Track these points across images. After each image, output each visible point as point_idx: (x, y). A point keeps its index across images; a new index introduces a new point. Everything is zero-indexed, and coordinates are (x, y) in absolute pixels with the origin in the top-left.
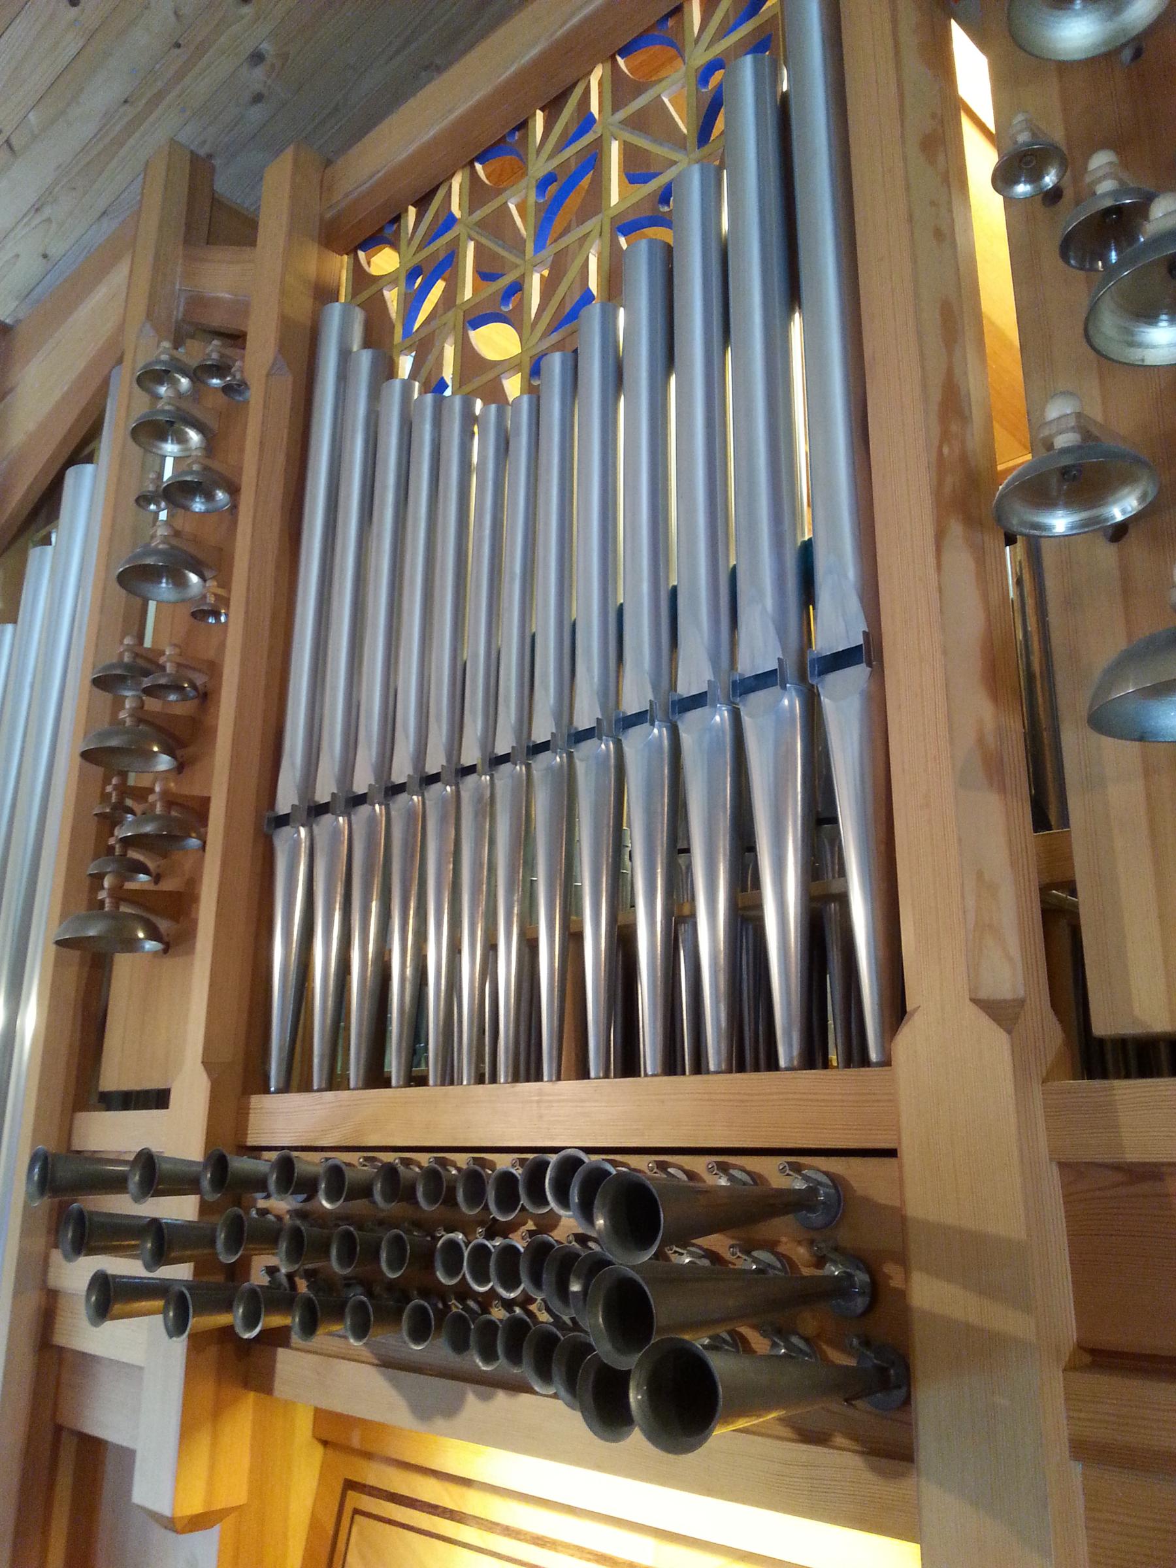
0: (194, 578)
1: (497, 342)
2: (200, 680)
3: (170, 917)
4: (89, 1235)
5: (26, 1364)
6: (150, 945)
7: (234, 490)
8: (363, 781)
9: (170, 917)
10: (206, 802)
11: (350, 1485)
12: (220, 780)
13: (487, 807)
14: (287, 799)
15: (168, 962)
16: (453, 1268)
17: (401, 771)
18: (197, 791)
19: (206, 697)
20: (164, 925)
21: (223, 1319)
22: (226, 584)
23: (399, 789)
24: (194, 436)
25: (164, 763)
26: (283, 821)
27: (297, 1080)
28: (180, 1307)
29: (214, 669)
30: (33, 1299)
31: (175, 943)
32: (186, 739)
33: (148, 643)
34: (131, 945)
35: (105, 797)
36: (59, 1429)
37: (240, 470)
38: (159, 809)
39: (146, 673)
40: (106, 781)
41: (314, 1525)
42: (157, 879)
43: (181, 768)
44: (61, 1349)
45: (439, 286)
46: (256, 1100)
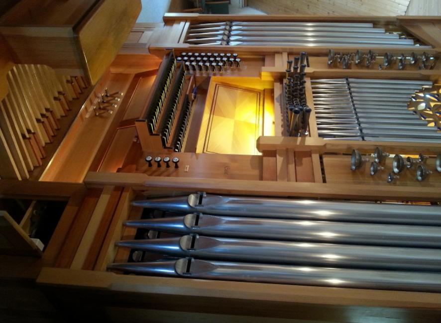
0: (387, 64)
1: (422, 106)
2: (370, 66)
3: (333, 65)
4: (296, 60)
5: (273, 51)
6: (329, 62)
7: (403, 69)
8: (352, 89)
9: (333, 65)
10: (351, 69)
11: (260, 93)
12: (354, 70)
13: (348, 104)
14: (350, 80)
15: (327, 65)
16: (295, 100)
17: (353, 94)
18: (352, 67)
19: (368, 67)
20: (332, 64)
21: (287, 76)
22: (386, 69)
23: (360, 125)
24: (413, 62)
25: (357, 62)
26: (347, 79)
27: (313, 83)
28: (289, 71)
29: (372, 68)
30: (281, 51)
31: (330, 66)
32: (360, 65)
33: (377, 57)
34: (330, 60)
35: (352, 54)
37: (406, 70)
38: (350, 62)
39: (371, 58)
40: (354, 53)
41: (255, 89)
42: (339, 62)
43: (356, 64)
44: (274, 55)
45: (436, 100)
46: (310, 78)
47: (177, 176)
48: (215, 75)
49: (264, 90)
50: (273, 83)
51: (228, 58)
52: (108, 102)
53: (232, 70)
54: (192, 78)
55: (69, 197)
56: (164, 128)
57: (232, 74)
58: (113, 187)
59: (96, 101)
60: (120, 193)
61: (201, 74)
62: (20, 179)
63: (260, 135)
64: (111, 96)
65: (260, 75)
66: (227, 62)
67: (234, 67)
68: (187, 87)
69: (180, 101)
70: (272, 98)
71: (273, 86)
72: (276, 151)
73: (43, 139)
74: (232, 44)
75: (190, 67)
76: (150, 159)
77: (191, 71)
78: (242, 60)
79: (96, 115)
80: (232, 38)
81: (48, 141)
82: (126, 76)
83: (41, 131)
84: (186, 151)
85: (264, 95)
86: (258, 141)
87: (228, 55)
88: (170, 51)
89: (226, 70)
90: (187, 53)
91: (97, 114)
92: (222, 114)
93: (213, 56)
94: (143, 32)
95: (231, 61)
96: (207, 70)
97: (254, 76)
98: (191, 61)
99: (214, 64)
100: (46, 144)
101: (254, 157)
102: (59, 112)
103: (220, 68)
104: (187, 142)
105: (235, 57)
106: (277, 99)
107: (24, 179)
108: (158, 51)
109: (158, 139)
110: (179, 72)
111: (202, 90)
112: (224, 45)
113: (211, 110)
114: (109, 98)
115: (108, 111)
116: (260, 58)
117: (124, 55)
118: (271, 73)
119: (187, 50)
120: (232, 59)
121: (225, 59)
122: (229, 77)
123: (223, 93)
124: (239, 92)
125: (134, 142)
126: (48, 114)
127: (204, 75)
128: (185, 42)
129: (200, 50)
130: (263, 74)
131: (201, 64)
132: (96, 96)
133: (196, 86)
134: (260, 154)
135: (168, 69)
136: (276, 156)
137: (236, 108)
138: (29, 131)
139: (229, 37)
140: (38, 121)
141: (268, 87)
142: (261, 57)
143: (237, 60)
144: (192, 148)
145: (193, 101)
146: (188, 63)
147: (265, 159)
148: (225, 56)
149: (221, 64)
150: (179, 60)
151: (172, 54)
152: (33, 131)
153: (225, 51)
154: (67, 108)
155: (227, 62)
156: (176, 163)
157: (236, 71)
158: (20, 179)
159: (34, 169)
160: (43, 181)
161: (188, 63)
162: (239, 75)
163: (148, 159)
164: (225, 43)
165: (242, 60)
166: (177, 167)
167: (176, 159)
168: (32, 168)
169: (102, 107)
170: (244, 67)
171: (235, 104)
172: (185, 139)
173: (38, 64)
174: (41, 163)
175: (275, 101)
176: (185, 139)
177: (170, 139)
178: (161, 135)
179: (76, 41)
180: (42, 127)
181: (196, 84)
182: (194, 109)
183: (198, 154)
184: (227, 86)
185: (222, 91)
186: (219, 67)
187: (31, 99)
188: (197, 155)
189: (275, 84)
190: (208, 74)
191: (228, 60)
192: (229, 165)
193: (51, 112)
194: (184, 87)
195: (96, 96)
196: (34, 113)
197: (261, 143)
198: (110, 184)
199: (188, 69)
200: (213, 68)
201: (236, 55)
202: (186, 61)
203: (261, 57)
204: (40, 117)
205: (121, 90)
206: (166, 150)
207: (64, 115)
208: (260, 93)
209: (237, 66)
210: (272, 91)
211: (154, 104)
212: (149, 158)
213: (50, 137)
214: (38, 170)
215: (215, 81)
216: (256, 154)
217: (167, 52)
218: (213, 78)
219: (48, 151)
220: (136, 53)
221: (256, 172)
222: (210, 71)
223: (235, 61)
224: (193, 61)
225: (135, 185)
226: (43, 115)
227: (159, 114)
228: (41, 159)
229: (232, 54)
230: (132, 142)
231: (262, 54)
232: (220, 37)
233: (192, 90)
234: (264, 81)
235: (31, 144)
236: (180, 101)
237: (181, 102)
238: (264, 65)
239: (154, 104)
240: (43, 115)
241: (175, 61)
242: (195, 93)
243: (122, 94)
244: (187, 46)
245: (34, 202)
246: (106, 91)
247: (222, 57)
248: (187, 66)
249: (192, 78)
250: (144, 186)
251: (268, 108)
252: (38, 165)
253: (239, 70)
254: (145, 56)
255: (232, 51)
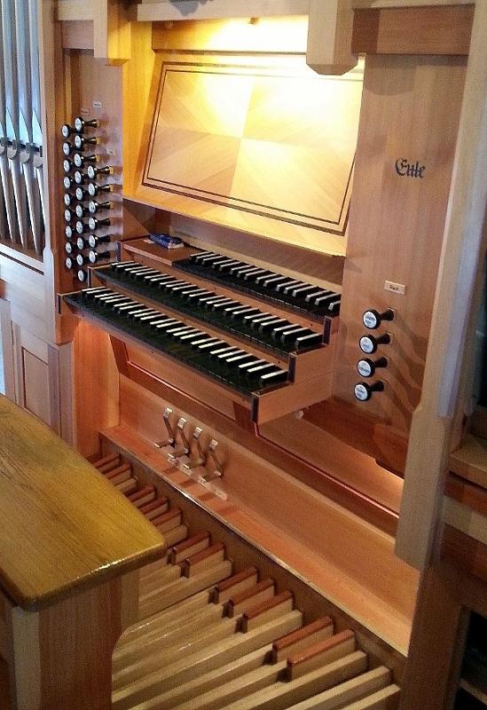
5: (51, 26)
11: (165, 63)
36: (64, 50)
44: (61, 22)
47: (425, 317)
48: (118, 188)
49: (156, 51)
50: (137, 25)
51: (73, 150)
52: (189, 446)
53: (105, 140)
54: (127, 247)
55: (464, 609)
56: (267, 337)
57: (116, 140)
58: (446, 499)
59: (185, 468)
60: (467, 487)
61: (118, 221)
62: (392, 689)
63: (303, 59)
64: (173, 435)
65: (118, 63)
66: (86, 154)
67: (96, 135)
68: (152, 263)
69: (186, 282)
70: (180, 26)
71: (145, 23)
72: (356, 10)
73: (284, 617)
74: (39, 139)
75: (101, 249)
76: (364, 389)
77: (112, 247)
78: (77, 113)
79: (220, 477)
80: (25, 139)
81: (289, 603)
82: (123, 390)
83: (266, 621)
84: (338, 280)
85: (170, 51)
86: (320, 69)
87: (66, 151)
88: (63, 303)
89: (105, 158)
90: (68, 255)
91: (220, 474)
92: (228, 174)
93: (71, 174)
94: (23, 348)
95: (81, 141)
96: (108, 207)
97: (120, 79)
98: (86, 212)
99: (91, 189)
100: (294, 608)
101: (368, 84)
102: (214, 567)
103: (103, 173)
104: (305, 272)
105: (72, 131)
106: (185, 13)
107: (391, 679)
108: (65, 330)
109: (303, 360)
110: (111, 283)
111: (158, 223)
112: (43, 159)
113: (214, 202)
114: (179, 438)
115: (211, 449)
116: (72, 66)
117: (79, 423)
118: (110, 30)
119: (60, 256)
120: (78, 141)
121: (78, 159)
122: (121, 148)
123: (167, 167)
124: (162, 123)
125: (303, 417)
126: (224, 597)
127: (121, 214)
128: (40, 257)
129: (59, 223)
130: (113, 55)
131: (92, 206)
132: (173, 469)
133: (149, 237)
134: (361, 64)
135: (109, 313)
136: (377, 10)
137: (208, 134)
138: (270, 659)
139: (23, 147)
140: (241, 627)
141: (147, 40)
142: (68, 58)
143: (78, 128)
144: (333, 266)
145: (187, 245)
146: (92, 256)
147: (383, 46)
148: (70, 158)
149: (91, 172)
150: (85, 274)
151: (73, 296)
152: (269, 648)
153: (58, 157)
154: (205, 543)
155: (86, 154)
156: (379, 318)
157: (108, 130)
158: (392, 689)
159: (363, 651)
160: (407, 647)
161: (92, 256)
162: (118, 121)
163: (364, 396)
164: (36, 157)
165: (77, 113)
166: (389, 316)
167: (370, 320)
168: (359, 655)
169: (200, 461)
170: (96, 107)
171: (196, 136)
172: (296, 275)
173: (109, 656)
174: (348, 633)
175: (190, 17)
176: (296, 275)
177: (297, 322)
178: (292, 354)
179: (43, 604)
180: (256, 619)
181: (145, 237)
182: (209, 248)
183: (348, 249)
184: (145, 156)
185: (157, 171)
186: (98, 176)
187: (190, 642)
188: (351, 254)
189: (140, 18)
190: (117, 204)
191: (80, 150)
192: (397, 165)
193: (218, 590)
194: (165, 288)
195: (173, 469)
196: (224, 636)
197: (329, 58)
198: (439, 504)
199: (106, 255)
200: (101, 191)
201: (65, 128)
202: (86, 260)
203: (69, 60)
204: (231, 623)
205: (162, 410)
206: (332, 337)
207: (221, 553)
208: (165, 63)
209: (95, 126)
210: (159, 27)
211: (204, 362)
212: (361, 392)
213: (278, 598)
214: (367, 644)
215: (135, 188)
216: (361, 76)
217: (65, 309)
218: (127, 194)
219: (318, 612)
220: (74, 417)
221: (426, 76)
222: (111, 198)
223: (80, 133)
224: (86, 243)
225: (447, 443)
226: (227, 613)
227: (232, 351)
228: (335, 632)
229: (68, 255)
230: (304, 420)
231: (60, 66)
232: (25, 169)
233: (159, 249)
234: (134, 49)
235: (302, 661)
236: (186, 282)
237: (193, 281)
238: (92, 51)
239: (204, 362)
240: (227, 613)
241: (89, 291)
242: (167, 238)
243: (169, 410)
244: (48, 253)
245: (465, 685)
246: (163, 445)
247: (73, 168)
248: (99, 257)
249: (127, 247)
250: (453, 422)
251: (205, 37)
252: (353, 640)
253: (104, 122)
254: (77, 352)
255: (57, 141)
